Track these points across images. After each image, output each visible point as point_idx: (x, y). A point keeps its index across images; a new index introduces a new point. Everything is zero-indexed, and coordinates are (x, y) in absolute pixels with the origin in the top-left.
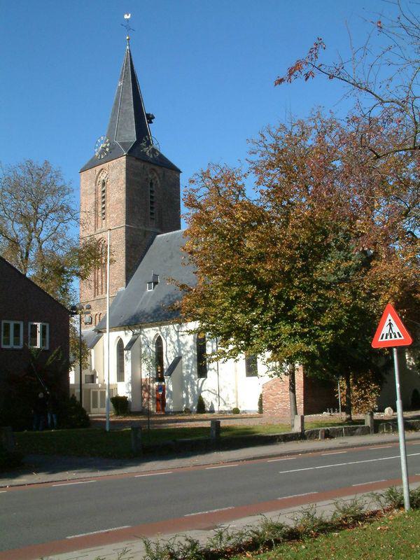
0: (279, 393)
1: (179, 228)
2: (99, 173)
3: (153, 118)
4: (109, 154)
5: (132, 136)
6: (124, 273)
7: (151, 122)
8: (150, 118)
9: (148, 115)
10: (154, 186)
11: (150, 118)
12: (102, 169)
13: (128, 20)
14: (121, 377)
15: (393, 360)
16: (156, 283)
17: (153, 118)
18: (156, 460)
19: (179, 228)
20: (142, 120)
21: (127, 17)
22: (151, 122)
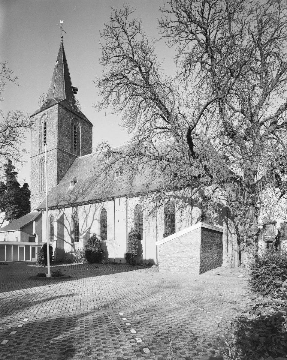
0: (176, 252)
1: (91, 152)
2: (42, 117)
3: (77, 90)
4: (48, 105)
5: (61, 95)
6: (56, 177)
7: (76, 93)
8: (76, 90)
9: (74, 88)
10: (76, 129)
11: (76, 90)
12: (44, 114)
13: (62, 24)
14: (51, 238)
15: (13, 254)
16: (75, 182)
17: (77, 90)
18: (124, 271)
19: (91, 152)
20: (71, 91)
21: (61, 22)
22: (76, 93)
